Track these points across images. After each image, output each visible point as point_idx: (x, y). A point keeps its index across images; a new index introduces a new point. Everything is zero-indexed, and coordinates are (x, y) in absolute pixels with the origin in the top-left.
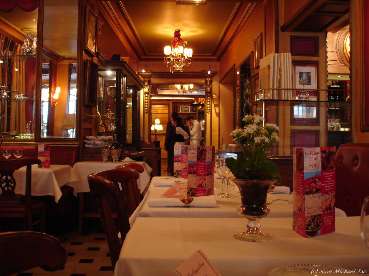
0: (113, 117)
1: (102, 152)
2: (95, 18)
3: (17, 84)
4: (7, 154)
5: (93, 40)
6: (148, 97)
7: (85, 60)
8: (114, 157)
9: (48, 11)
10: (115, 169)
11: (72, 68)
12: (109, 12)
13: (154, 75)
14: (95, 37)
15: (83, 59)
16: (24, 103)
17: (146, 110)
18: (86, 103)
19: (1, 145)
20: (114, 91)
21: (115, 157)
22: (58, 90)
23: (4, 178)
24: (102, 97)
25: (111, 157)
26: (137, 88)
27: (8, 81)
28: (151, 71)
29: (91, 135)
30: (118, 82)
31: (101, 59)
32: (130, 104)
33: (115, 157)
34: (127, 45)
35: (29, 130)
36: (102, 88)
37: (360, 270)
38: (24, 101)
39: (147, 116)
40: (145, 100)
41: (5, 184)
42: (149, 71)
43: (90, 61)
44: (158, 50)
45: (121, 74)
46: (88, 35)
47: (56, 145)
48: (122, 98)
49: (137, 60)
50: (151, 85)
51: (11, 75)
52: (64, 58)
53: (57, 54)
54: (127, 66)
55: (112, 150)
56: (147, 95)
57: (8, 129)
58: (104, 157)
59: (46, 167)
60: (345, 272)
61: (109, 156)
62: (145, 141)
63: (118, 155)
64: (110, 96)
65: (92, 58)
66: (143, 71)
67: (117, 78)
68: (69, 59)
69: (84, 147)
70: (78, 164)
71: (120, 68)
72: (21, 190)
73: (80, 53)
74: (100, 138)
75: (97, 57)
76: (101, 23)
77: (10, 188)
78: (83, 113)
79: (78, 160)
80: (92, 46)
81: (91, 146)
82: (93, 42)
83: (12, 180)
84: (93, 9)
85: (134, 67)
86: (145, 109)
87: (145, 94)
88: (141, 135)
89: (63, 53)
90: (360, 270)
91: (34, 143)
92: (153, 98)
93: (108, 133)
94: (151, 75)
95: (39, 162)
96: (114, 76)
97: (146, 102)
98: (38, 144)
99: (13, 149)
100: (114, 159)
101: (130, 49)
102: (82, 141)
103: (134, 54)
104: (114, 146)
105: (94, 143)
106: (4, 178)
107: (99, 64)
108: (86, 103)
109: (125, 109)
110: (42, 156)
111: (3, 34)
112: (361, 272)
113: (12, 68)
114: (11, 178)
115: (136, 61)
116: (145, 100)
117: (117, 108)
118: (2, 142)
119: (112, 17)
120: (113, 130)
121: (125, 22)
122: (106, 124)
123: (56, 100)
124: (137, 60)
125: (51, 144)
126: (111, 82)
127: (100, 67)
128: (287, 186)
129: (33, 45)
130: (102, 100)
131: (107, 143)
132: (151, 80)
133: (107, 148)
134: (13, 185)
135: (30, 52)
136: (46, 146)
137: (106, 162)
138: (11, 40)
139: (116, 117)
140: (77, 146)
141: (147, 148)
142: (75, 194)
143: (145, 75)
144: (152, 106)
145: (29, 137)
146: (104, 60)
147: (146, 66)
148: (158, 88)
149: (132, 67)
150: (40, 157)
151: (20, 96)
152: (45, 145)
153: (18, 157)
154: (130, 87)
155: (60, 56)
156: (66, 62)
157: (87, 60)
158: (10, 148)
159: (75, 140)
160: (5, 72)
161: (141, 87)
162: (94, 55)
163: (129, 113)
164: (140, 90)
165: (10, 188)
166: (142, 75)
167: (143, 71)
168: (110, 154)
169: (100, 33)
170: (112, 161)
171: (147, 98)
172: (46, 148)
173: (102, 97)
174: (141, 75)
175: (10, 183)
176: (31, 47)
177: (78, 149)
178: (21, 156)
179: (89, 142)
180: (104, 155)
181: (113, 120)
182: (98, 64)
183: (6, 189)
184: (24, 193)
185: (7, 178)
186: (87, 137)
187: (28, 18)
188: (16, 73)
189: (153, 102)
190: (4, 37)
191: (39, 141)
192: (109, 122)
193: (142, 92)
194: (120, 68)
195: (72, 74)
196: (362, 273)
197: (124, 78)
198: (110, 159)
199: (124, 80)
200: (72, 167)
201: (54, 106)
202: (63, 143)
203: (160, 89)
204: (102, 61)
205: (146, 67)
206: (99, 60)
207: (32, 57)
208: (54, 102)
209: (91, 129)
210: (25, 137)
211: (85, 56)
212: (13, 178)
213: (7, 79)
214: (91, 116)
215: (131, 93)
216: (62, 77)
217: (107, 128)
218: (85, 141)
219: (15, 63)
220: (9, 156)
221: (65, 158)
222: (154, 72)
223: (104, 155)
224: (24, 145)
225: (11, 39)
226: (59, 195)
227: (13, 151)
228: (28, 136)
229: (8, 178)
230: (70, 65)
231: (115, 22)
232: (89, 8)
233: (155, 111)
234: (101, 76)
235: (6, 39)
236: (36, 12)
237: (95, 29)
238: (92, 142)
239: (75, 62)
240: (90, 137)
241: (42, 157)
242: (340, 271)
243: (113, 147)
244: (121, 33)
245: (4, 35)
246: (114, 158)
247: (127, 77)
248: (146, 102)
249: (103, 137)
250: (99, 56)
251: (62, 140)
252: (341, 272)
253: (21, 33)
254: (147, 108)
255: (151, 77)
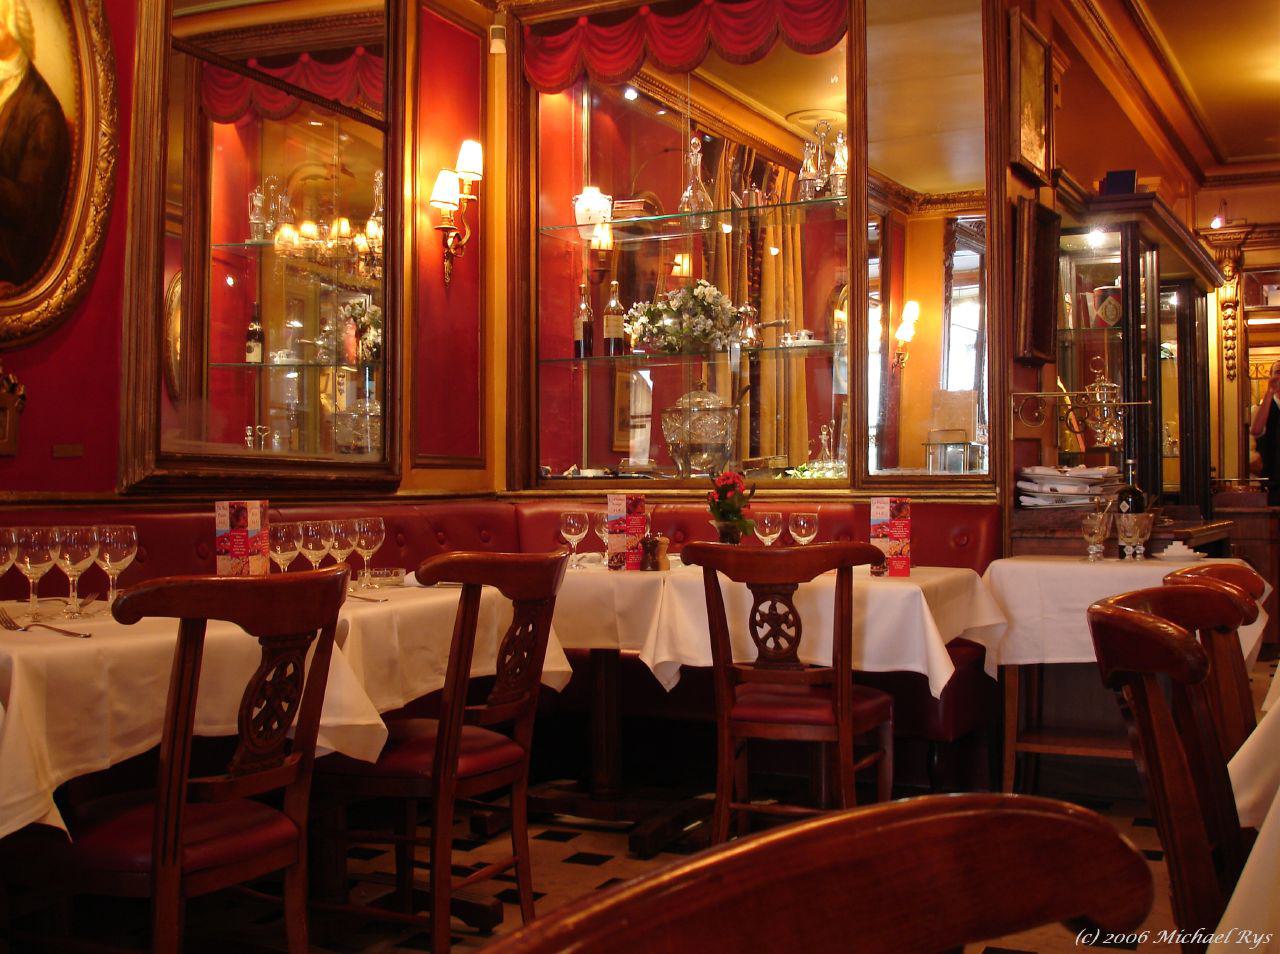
0: (1114, 396)
1: (1084, 522)
2: (1042, 50)
3: (777, 300)
4: (767, 530)
5: (1038, 127)
6: (1234, 318)
7: (1015, 200)
8: (1130, 540)
9: (880, 43)
10: (1159, 584)
11: (955, 231)
12: (1088, 21)
13: (1254, 235)
14: (1047, 116)
15: (1008, 196)
16: (802, 361)
17: (1229, 368)
18: (1022, 351)
19: (751, 500)
20: (1113, 302)
21: (1131, 542)
22: (912, 309)
23: (765, 607)
24: (1071, 327)
25: (1117, 539)
26: (1194, 288)
27: (751, 289)
28: (1243, 222)
29: (1040, 464)
30: (1130, 269)
31: (1067, 192)
32: (1170, 347)
33: (1131, 542)
34: (1154, 134)
35: (830, 451)
36: (1071, 293)
37: (1247, 933)
38: (800, 355)
39: (1232, 388)
40: (1224, 328)
41: (767, 628)
42: (1234, 223)
43: (1030, 201)
44: (1270, 139)
45: (1141, 242)
46: (1021, 112)
47: (922, 501)
48: (1143, 327)
49: (1189, 183)
50: (1244, 274)
51: (758, 269)
52: (929, 201)
53: (904, 189)
54: (1161, 211)
55: (1120, 517)
56: (1229, 311)
57: (755, 451)
58: (1093, 539)
59: (895, 573)
60: (1194, 938)
61: (1107, 536)
62: (1228, 484)
63: (1142, 536)
64: (1101, 322)
65: (1037, 193)
66: (1217, 224)
67: (1124, 256)
68: (945, 200)
69: (1018, 505)
70: (997, 565)
71: (1133, 217)
72: (819, 651)
73: (995, 179)
74: (1071, 471)
75: (1055, 185)
76: (1060, 67)
77: (784, 643)
78: (1011, 387)
79: (998, 554)
80: (1036, 148)
81: (1040, 502)
82: (1039, 134)
83: (791, 617)
84: (1033, 18)
85: (1181, 210)
86: (1225, 362)
87: (1224, 307)
88: (1214, 462)
89: (922, 184)
90: (1247, 933)
91: (847, 492)
92: (1252, 322)
93: (1093, 457)
94: (1243, 236)
95: (876, 559)
96: (1112, 249)
97: (1227, 339)
98: (869, 497)
99: (786, 515)
100: (1129, 550)
101: (1163, 146)
102: (1012, 486)
103: (1178, 163)
104: (1128, 502)
105: (1053, 490)
106: (765, 607)
107: (1059, 210)
108: (1022, 351)
109: (1156, 362)
110: (884, 536)
111: (732, 137)
112: (1251, 938)
113: (762, 248)
114: (787, 609)
115: (1186, 186)
116: (1224, 328)
117: (1129, 366)
118: (752, 492)
119: (1100, 41)
120: (1111, 445)
121: (1145, 53)
122: (1090, 422)
123: (906, 344)
124: (1189, 183)
125: (912, 497)
126: (1104, 273)
127: (1067, 221)
128: (699, 564)
129: (834, 165)
130: (1070, 338)
131: (1098, 489)
132: (1246, 254)
133: (1101, 508)
134: (792, 632)
135: (827, 187)
136: (895, 502)
137: (1099, 559)
138: (754, 155)
139: (1127, 397)
140: (995, 501)
141: (1239, 509)
142: (991, 670)
143: (1221, 237)
144: (1252, 351)
145: (830, 475)
146: (1076, 196)
147: (1225, 204)
148: (1271, 283)
149: (1174, 209)
150: (877, 540)
151: (797, 339)
152: (894, 499)
153: (804, 541)
154: (1165, 285)
155: (915, 193)
156: (936, 214)
157: (1021, 199)
158: (778, 509)
159: (988, 483)
160: (741, 266)
161: (1208, 284)
162: (1045, 179)
163: (1170, 374)
164: (1204, 294)
165: (784, 643)
166: (1211, 238)
167: (1217, 224)
168: (1114, 528)
169: (1057, 100)
170: (1122, 556)
171: (1230, 322)
172: (897, 510)
173: (1071, 327)
174: (1205, 238)
175: (784, 627)
176: (828, 173)
177: (995, 513)
178: (812, 537)
179: (1035, 488)
180: (1091, 534)
181: (1114, 409)
182: (1058, 211)
183: (770, 643)
184: (825, 658)
185: (773, 608)
186: (1028, 471)
187: (813, 78)
188: (773, 260)
189: (1252, 338)
190: (733, 145)
191: (864, 486)
192: (1098, 416)
193: (1213, 300)
194: (1133, 217)
195: (957, 253)
196: (1253, 944)
197: (1148, 253)
198: (1113, 549)
199: (1149, 259)
200: (981, 575)
201: (898, 365)
202: (946, 493)
203: (1275, 287)
204: (1070, 199)
205: (1223, 207)
206: (1059, 198)
207: (832, 207)
208: (899, 355)
209: (1037, 442)
210: (816, 475)
211: (1013, 187)
212: (792, 610)
213: (746, 283)
214: (1039, 395)
215: (1171, 307)
216: (921, 268)
217: (1089, 435)
218: (1021, 484)
219: (770, 229)
220: (776, 536)
221: (952, 544)
222: (1255, 226)
223: (1091, 535)
224: (815, 500)
225: (754, 151)
226: (941, 673)
227: (786, 522)
228: (830, 470)
229: (775, 609)
230: (951, 221)
231: (1111, 55)
232: (1021, 17)
233: (1257, 368)
234: (1064, 253)
235: (741, 151)
236: (840, 52)
237: (1043, 87)
238: (1046, 488)
239: (965, 210)
240: (1039, 470)
241: (885, 539)
242: (1175, 937)
243: (1125, 506)
244: (1129, 92)
245: (732, 141)
246: (1130, 544)
247: (1162, 251)
248: (1227, 339)
249: (1081, 470)
250: (1062, 183)
251: (936, 482)
252: (1181, 939)
253: (784, 129)
254: (1233, 358)
255: (1243, 243)
